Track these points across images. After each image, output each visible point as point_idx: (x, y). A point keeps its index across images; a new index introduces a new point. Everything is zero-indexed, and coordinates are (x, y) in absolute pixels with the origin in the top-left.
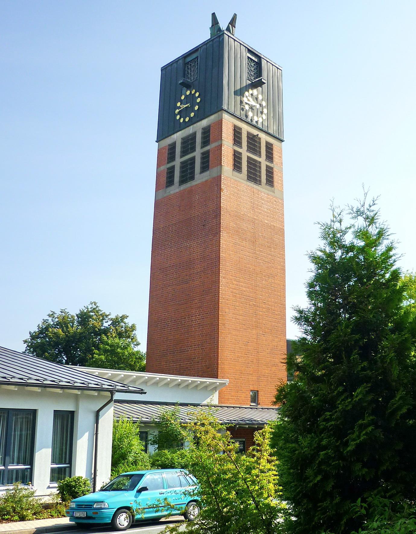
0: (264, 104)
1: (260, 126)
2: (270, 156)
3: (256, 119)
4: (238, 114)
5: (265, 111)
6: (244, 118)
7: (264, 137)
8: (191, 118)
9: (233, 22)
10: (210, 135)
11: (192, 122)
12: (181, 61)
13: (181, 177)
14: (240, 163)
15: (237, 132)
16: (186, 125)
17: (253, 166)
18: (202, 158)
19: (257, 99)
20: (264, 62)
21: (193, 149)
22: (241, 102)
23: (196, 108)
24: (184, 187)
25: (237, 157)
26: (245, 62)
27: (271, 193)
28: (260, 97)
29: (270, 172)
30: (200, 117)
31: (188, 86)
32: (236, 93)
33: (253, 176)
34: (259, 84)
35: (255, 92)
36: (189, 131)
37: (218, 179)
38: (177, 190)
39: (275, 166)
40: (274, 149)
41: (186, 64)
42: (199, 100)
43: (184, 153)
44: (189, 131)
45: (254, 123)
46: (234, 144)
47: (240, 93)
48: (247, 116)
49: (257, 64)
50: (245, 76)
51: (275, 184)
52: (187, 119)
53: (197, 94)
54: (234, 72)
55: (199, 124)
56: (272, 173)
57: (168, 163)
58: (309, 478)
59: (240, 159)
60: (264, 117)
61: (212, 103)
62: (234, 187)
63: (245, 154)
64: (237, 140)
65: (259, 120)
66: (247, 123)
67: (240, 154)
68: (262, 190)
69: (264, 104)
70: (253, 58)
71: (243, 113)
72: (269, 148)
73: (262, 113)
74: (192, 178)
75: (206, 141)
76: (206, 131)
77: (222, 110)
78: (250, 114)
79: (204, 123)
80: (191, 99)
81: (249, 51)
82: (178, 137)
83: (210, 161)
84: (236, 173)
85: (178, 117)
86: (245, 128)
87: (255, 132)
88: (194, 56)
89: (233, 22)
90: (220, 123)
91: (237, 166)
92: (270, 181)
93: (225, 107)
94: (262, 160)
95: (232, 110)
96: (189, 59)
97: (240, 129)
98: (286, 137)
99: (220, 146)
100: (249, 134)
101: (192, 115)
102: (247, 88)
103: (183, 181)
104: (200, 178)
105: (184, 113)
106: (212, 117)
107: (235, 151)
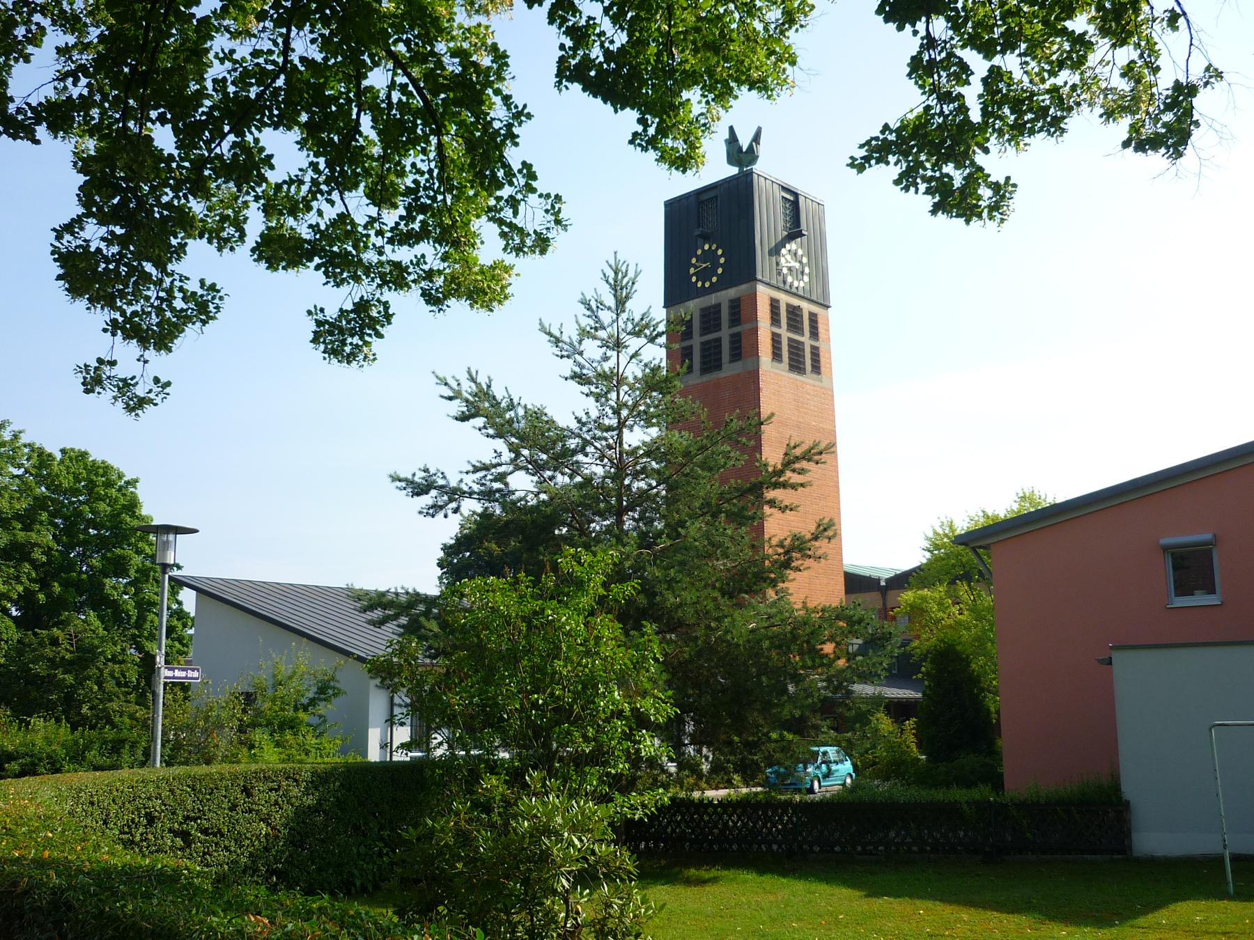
0: (805, 260)
1: (801, 293)
2: (814, 334)
3: (796, 284)
4: (774, 282)
5: (807, 270)
6: (781, 285)
7: (806, 307)
8: (712, 283)
9: (757, 138)
10: (742, 312)
11: (714, 288)
12: (692, 199)
13: (703, 363)
14: (780, 349)
15: (774, 305)
16: (704, 292)
17: (796, 348)
18: (732, 342)
19: (795, 254)
20: (801, 199)
21: (718, 327)
22: (778, 264)
23: (720, 271)
24: (707, 378)
25: (776, 339)
26: (779, 204)
27: (818, 383)
28: (800, 252)
29: (815, 353)
30: (724, 283)
31: (706, 238)
32: (770, 254)
33: (796, 365)
34: (800, 234)
35: (792, 246)
36: (712, 299)
37: (754, 376)
38: (698, 381)
39: (821, 344)
40: (820, 320)
41: (700, 203)
42: (722, 260)
43: (705, 330)
44: (712, 299)
45: (794, 290)
46: (772, 324)
47: (775, 251)
48: (785, 282)
49: (793, 203)
50: (780, 224)
51: (823, 369)
52: (707, 285)
53: (720, 252)
54: (768, 219)
55: (723, 293)
56: (818, 355)
57: (683, 340)
58: (628, 832)
59: (780, 343)
60: (806, 279)
61: (742, 268)
62: (775, 381)
63: (785, 333)
64: (775, 320)
65: (800, 284)
66: (786, 291)
67: (779, 336)
68: (808, 380)
69: (805, 260)
70: (788, 197)
71: (781, 278)
72: (813, 318)
73: (802, 273)
74: (719, 367)
75: (736, 319)
76: (735, 305)
77: (756, 280)
78: (790, 279)
79: (732, 293)
80: (710, 256)
81: (784, 189)
82: (693, 307)
83: (743, 347)
84: (776, 364)
85: (694, 279)
86: (784, 299)
87: (795, 302)
88: (712, 194)
89: (757, 138)
90: (753, 297)
91: (777, 355)
92: (816, 368)
93: (759, 277)
94: (806, 339)
95: (767, 279)
96: (704, 197)
97: (778, 301)
98: (834, 300)
99: (756, 329)
100: (788, 305)
101: (714, 279)
102: (782, 244)
103: (706, 369)
104: (729, 369)
105: (704, 275)
106: (744, 287)
107: (774, 334)
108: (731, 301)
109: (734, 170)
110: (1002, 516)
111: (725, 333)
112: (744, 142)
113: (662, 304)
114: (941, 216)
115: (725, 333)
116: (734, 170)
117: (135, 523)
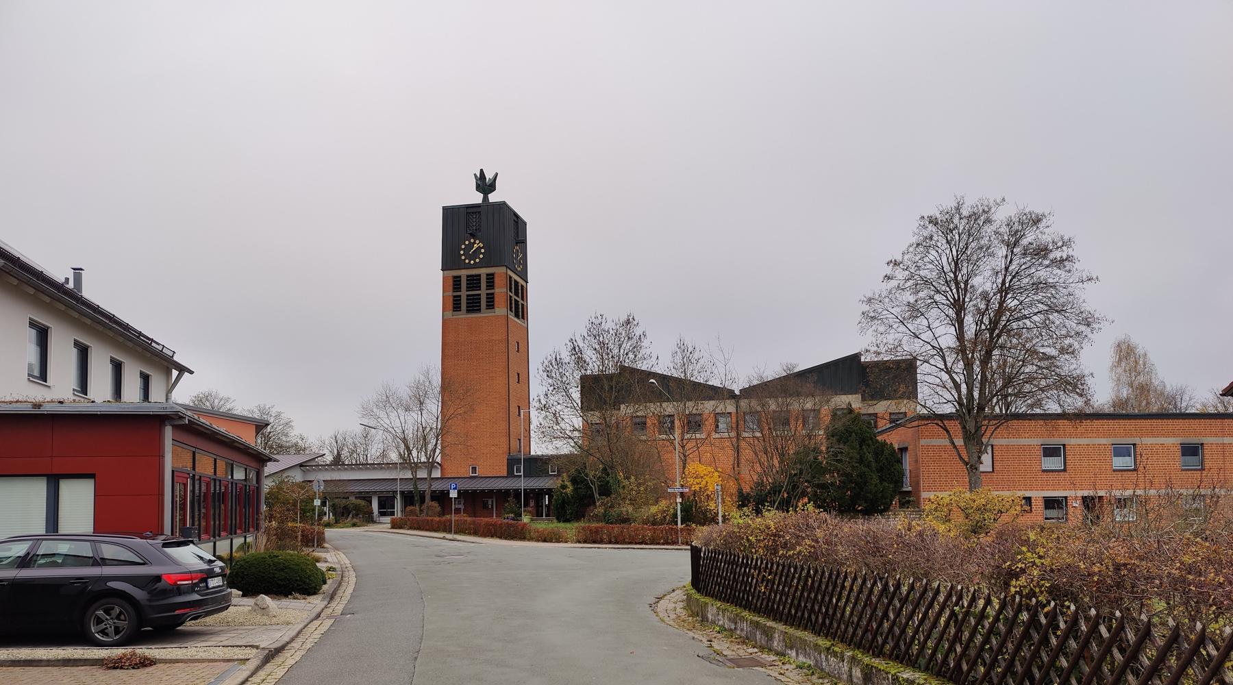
16: (469, 267)
21: (479, 288)
33: (517, 316)
109: (478, 198)
111: (483, 292)
112: (489, 176)
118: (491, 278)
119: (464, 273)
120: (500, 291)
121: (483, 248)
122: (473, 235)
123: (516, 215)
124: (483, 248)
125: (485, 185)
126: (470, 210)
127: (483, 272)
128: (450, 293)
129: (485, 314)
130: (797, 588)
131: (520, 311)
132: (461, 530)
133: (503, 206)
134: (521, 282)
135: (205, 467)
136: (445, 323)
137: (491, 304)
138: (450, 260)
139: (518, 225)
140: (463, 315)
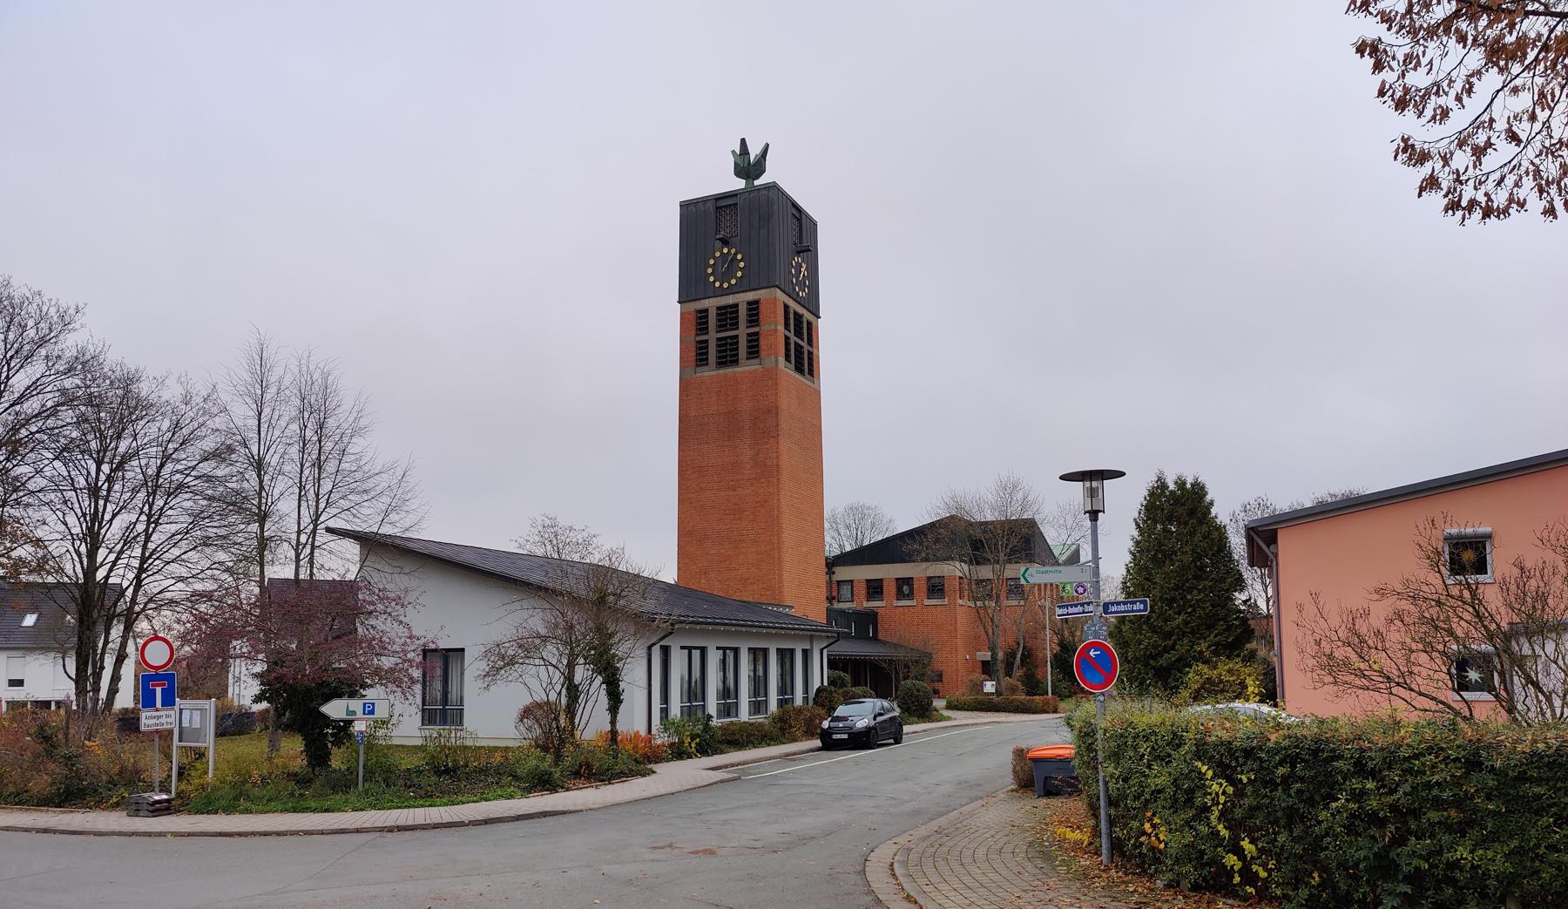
12: (710, 205)
16: (723, 292)
21: (735, 325)
33: (799, 369)
42: (710, 271)
43: (721, 327)
53: (742, 265)
79: (751, 296)
88: (730, 201)
92: (811, 372)
108: (749, 303)
109: (740, 184)
110: (989, 517)
111: (742, 331)
112: (754, 152)
113: (677, 298)
114: (68, 301)
115: (742, 331)
116: (740, 184)
117: (573, 616)
118: (754, 306)
119: (711, 304)
120: (775, 331)
121: (746, 271)
122: (725, 242)
123: (795, 206)
124: (746, 271)
125: (748, 166)
126: (722, 204)
127: (743, 298)
128: (692, 337)
129: (746, 368)
130: (121, 658)
131: (804, 362)
132: (314, 811)
133: (773, 187)
134: (807, 316)
135: (60, 736)
136: (686, 388)
137: (754, 351)
138: (691, 285)
139: (801, 232)
140: (709, 373)
